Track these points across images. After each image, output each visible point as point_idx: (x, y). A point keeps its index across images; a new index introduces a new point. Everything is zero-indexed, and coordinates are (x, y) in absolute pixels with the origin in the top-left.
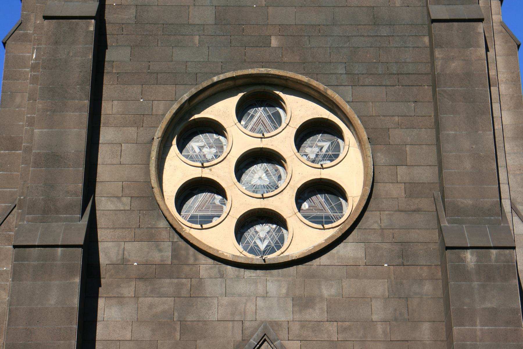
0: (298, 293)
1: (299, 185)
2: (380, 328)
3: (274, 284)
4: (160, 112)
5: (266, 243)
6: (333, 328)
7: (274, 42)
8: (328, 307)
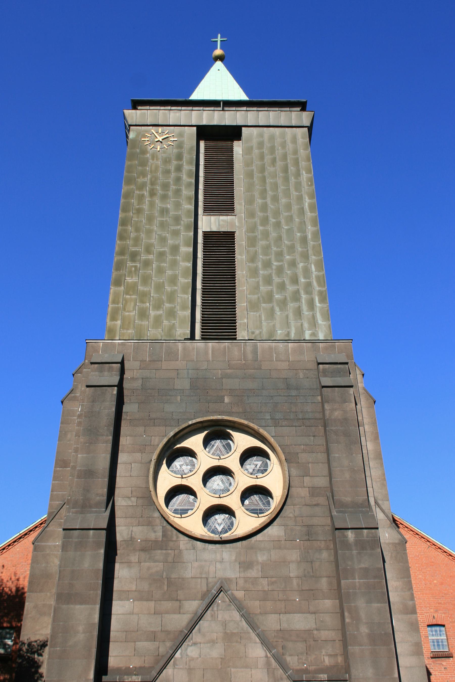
2: (295, 582)
4: (156, 443)
6: (265, 582)
7: (227, 400)
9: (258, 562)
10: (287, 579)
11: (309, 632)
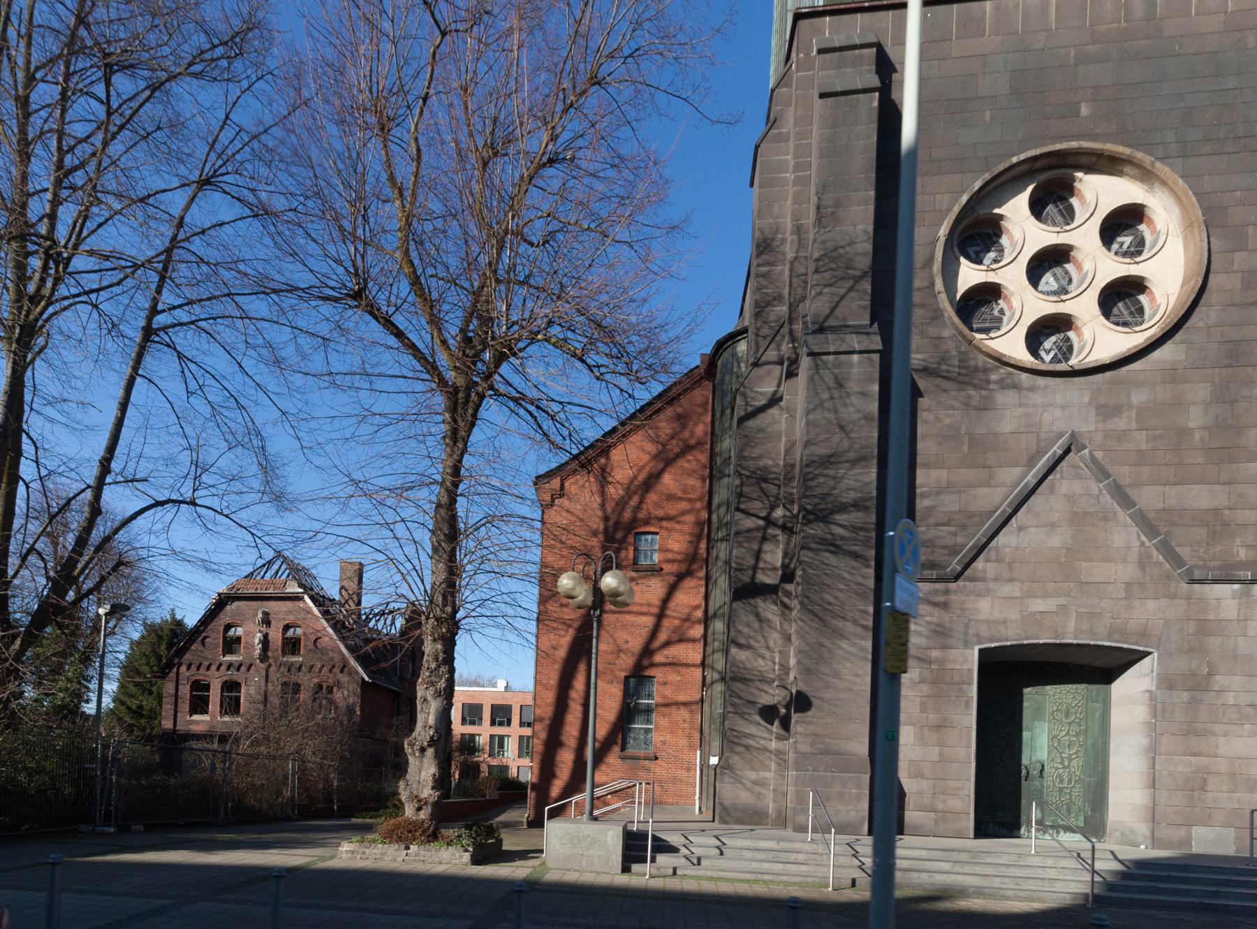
0: (1102, 401)
1: (1103, 284)
2: (1197, 436)
3: (1074, 392)
4: (945, 207)
5: (1052, 354)
6: (1142, 436)
7: (1085, 110)
8: (1138, 414)
9: (1130, 406)
10: (1185, 432)
11: (1216, 511)
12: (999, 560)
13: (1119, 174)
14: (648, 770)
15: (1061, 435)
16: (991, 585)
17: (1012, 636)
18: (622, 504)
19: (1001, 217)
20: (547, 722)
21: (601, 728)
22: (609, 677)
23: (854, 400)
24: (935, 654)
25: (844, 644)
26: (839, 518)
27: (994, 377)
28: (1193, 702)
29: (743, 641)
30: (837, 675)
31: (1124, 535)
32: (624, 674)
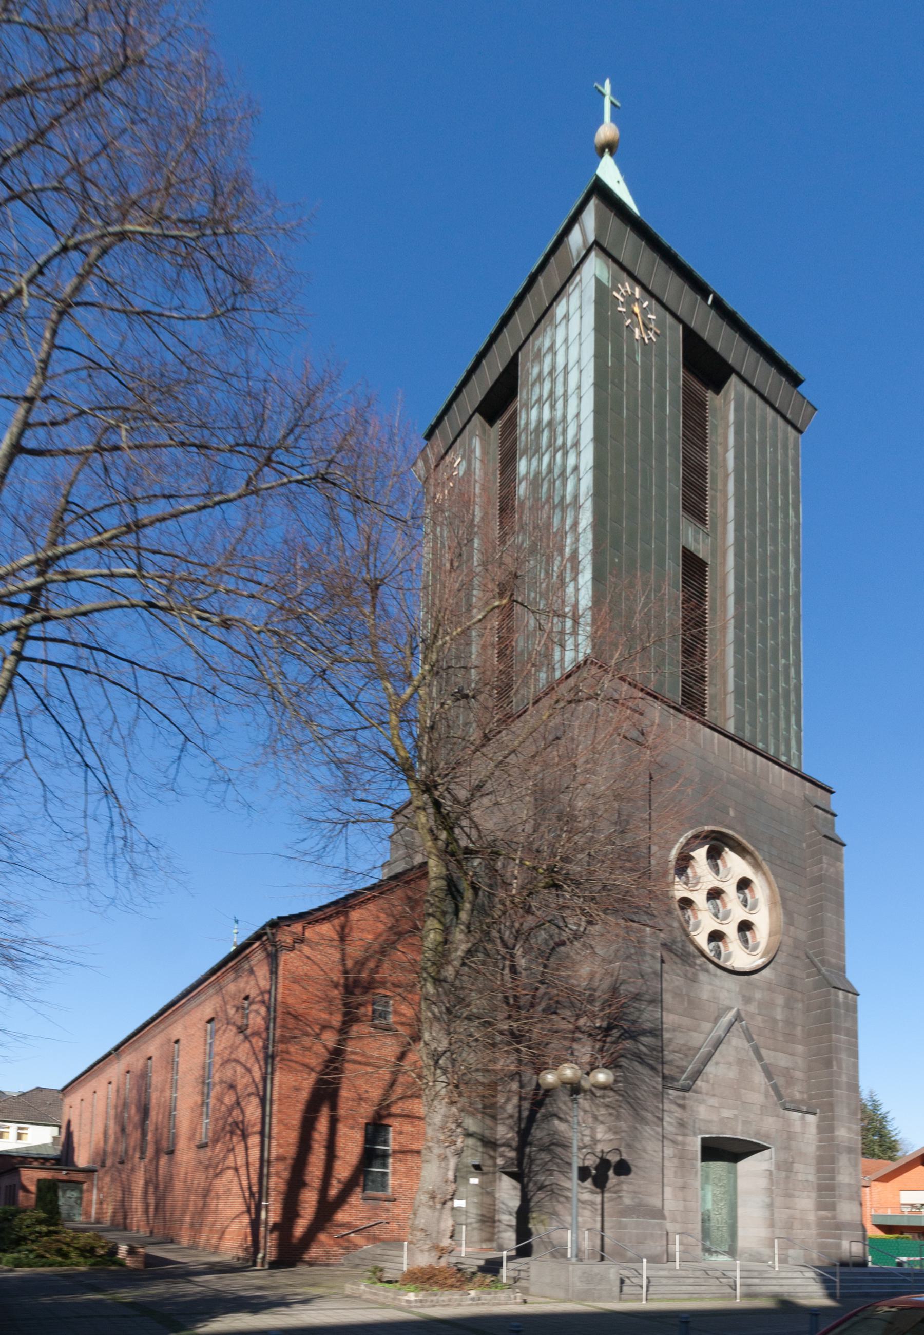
2: (780, 1024)
6: (759, 1018)
12: (707, 1082)
13: (743, 858)
14: (387, 1210)
15: (730, 1009)
16: (705, 1097)
17: (715, 1132)
18: (361, 964)
19: (692, 858)
20: (289, 1162)
21: (343, 1171)
22: (351, 1122)
23: (648, 958)
24: (680, 1138)
25: (647, 1128)
26: (644, 1039)
27: (698, 962)
28: (787, 1178)
29: (562, 1116)
30: (645, 1151)
31: (759, 1078)
32: (364, 1121)
